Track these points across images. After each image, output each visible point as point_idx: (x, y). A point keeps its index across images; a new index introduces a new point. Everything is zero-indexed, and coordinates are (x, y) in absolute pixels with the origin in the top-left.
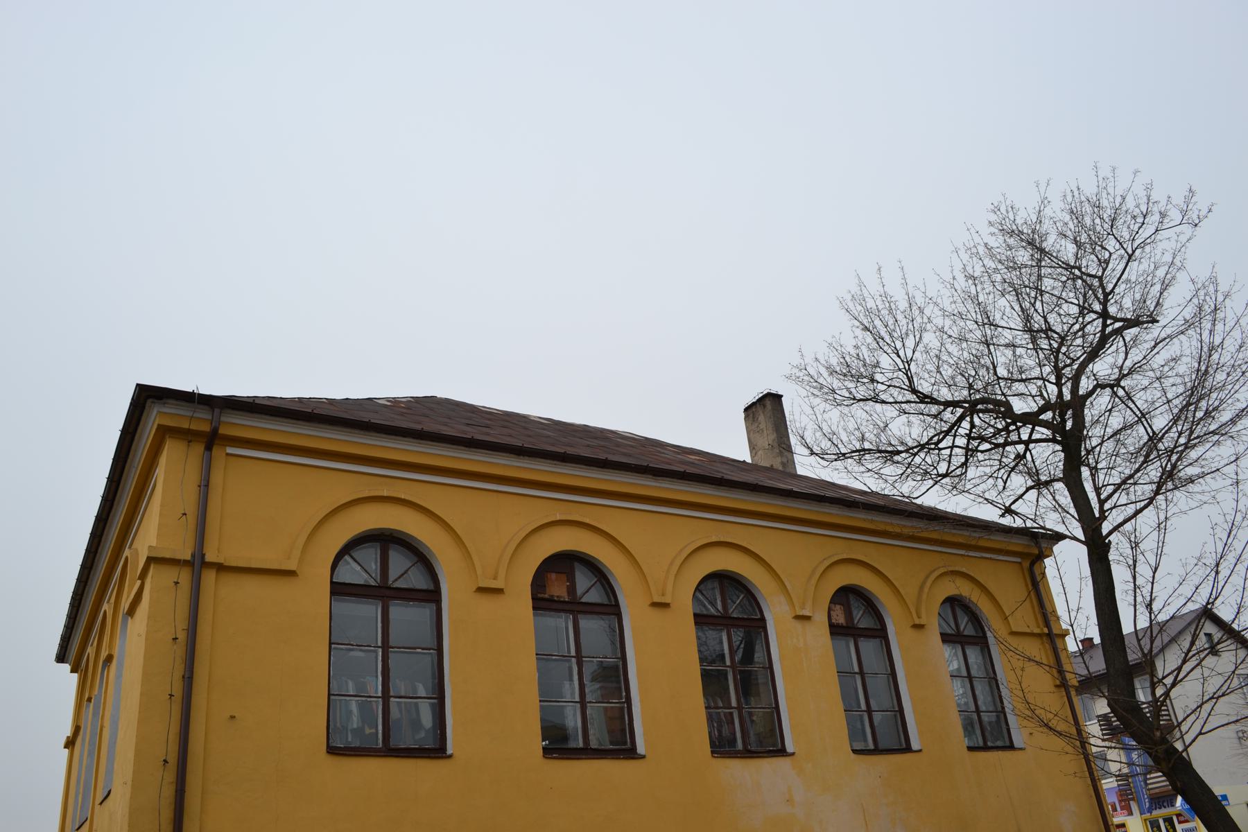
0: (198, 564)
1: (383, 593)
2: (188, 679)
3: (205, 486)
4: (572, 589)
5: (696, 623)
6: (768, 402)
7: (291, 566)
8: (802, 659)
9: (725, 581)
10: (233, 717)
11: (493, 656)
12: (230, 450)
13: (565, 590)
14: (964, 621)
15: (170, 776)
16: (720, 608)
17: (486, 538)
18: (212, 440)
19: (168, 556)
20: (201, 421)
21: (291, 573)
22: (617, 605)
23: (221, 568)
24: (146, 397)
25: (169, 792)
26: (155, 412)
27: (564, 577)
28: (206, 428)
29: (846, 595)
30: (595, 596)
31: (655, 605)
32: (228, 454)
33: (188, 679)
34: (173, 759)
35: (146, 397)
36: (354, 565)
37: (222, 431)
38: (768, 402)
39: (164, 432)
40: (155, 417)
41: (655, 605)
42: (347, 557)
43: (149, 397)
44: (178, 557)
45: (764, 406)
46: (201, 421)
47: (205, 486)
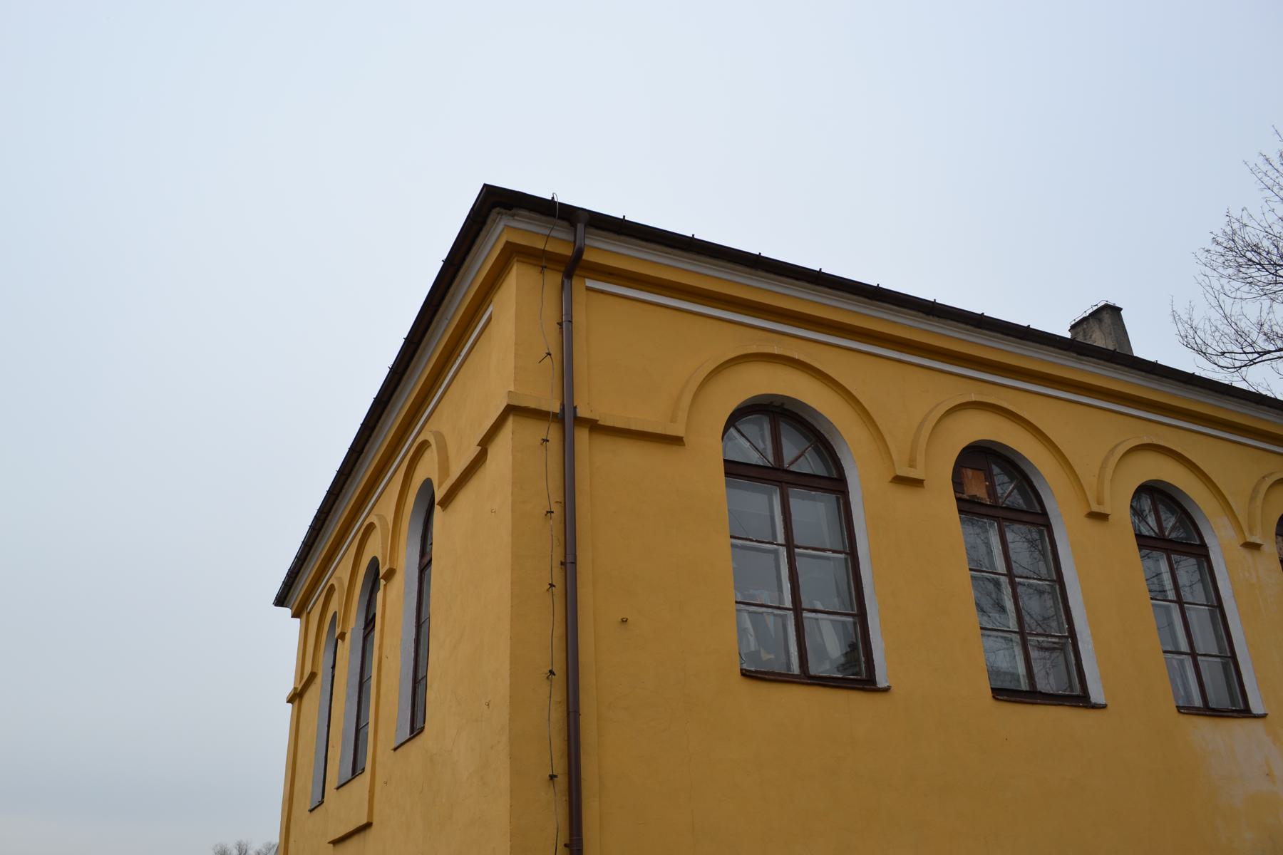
0: (568, 420)
1: (774, 476)
2: (569, 564)
3: (565, 324)
4: (992, 491)
5: (960, 511)
6: (1106, 317)
7: (677, 430)
8: (1100, 569)
9: (775, 412)
10: (624, 621)
11: (915, 553)
12: (590, 283)
13: (984, 491)
14: (1170, 522)
15: (559, 695)
16: (771, 458)
17: (896, 425)
18: (572, 267)
19: (532, 405)
20: (558, 242)
21: (677, 441)
22: (1044, 513)
23: (595, 427)
24: (493, 202)
25: (558, 714)
26: (501, 227)
27: (981, 474)
28: (567, 251)
29: (980, 457)
30: (810, 465)
31: (899, 480)
32: (588, 289)
33: (569, 564)
34: (559, 669)
35: (493, 202)
36: (742, 441)
37: (587, 256)
38: (1106, 317)
39: (513, 252)
40: (502, 232)
41: (899, 480)
42: (732, 430)
43: (494, 205)
44: (545, 408)
45: (1100, 321)
46: (558, 242)
47: (565, 324)
